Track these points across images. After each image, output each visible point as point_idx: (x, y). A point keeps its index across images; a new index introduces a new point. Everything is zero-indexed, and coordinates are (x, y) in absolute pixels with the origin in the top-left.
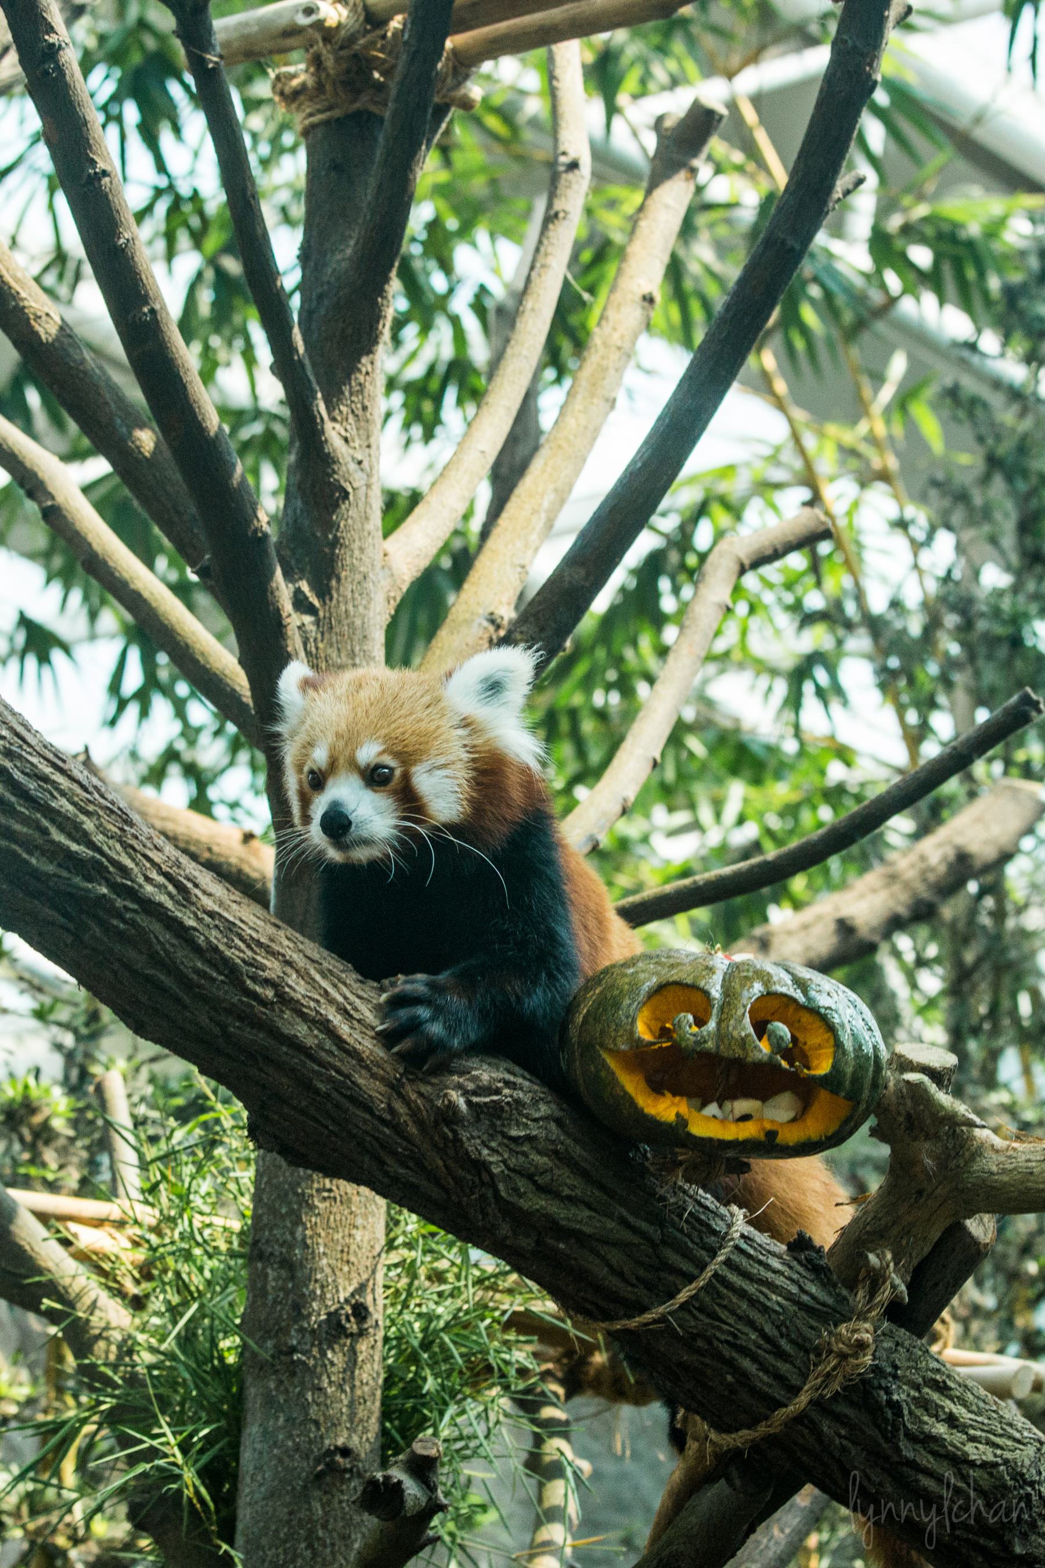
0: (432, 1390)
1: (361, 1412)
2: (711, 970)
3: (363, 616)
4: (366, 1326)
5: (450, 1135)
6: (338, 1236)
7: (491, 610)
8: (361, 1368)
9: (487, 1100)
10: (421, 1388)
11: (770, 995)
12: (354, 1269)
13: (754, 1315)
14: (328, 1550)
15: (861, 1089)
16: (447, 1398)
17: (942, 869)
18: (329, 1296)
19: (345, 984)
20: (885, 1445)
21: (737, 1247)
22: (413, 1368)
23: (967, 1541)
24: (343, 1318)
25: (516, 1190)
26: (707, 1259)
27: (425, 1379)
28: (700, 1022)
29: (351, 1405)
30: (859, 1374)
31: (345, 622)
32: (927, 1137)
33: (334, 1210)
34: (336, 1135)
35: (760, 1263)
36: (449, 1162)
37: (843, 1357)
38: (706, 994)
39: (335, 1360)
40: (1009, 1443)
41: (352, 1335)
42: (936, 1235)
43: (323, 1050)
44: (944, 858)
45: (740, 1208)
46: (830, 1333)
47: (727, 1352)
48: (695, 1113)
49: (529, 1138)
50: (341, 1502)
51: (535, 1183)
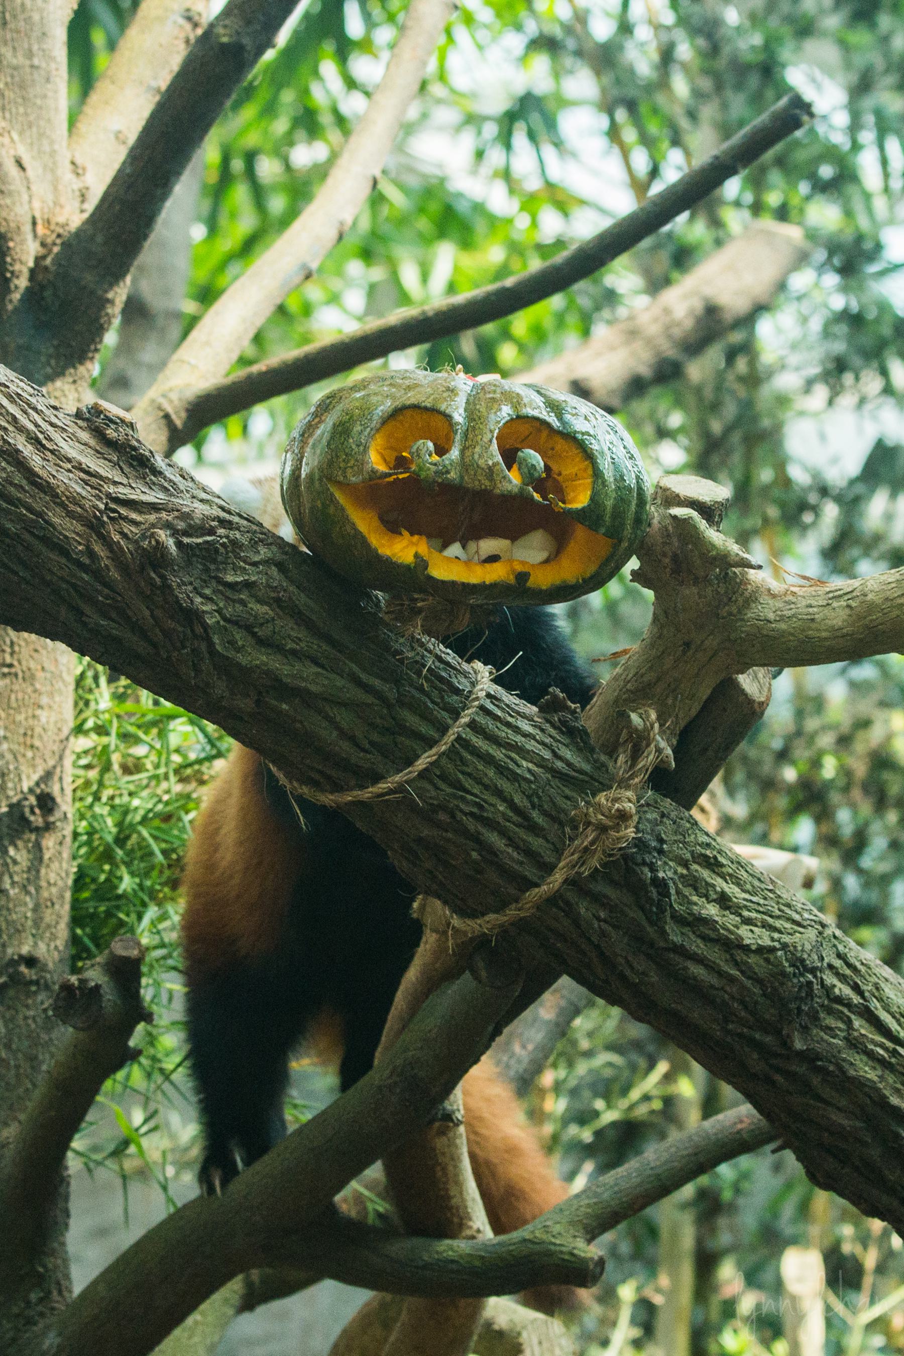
0: (129, 890)
1: (48, 916)
2: (452, 391)
3: (41, 10)
4: (51, 819)
5: (158, 580)
6: (20, 717)
7: (188, 5)
8: (48, 866)
9: (200, 540)
10: (116, 887)
11: (521, 418)
12: (38, 754)
13: (504, 784)
14: (13, 1072)
15: (623, 525)
16: (146, 899)
17: (689, 324)
18: (10, 785)
19: (35, 409)
20: (649, 929)
21: (482, 708)
22: (107, 867)
23: (741, 1036)
24: (27, 811)
25: (232, 643)
26: (450, 721)
27: (121, 879)
28: (441, 451)
29: (36, 909)
30: (621, 849)
31: (21, 17)
32: (696, 581)
33: (16, 687)
34: (27, 583)
35: (508, 725)
36: (159, 613)
37: (603, 829)
38: (448, 417)
39: (18, 858)
40: (788, 925)
41: (37, 830)
42: (705, 693)
43: (11, 484)
44: (691, 311)
45: (485, 664)
46: (588, 803)
47: (471, 825)
48: (435, 554)
49: (248, 585)
50: (26, 1018)
51: (254, 635)
